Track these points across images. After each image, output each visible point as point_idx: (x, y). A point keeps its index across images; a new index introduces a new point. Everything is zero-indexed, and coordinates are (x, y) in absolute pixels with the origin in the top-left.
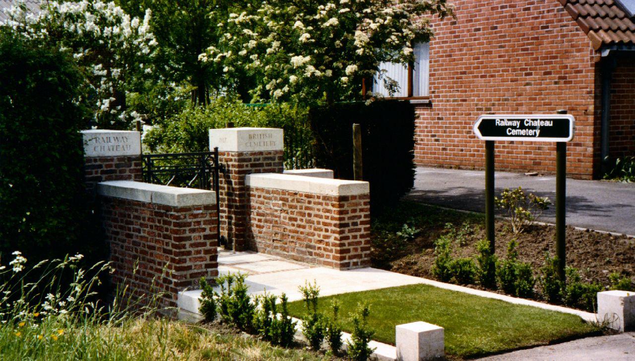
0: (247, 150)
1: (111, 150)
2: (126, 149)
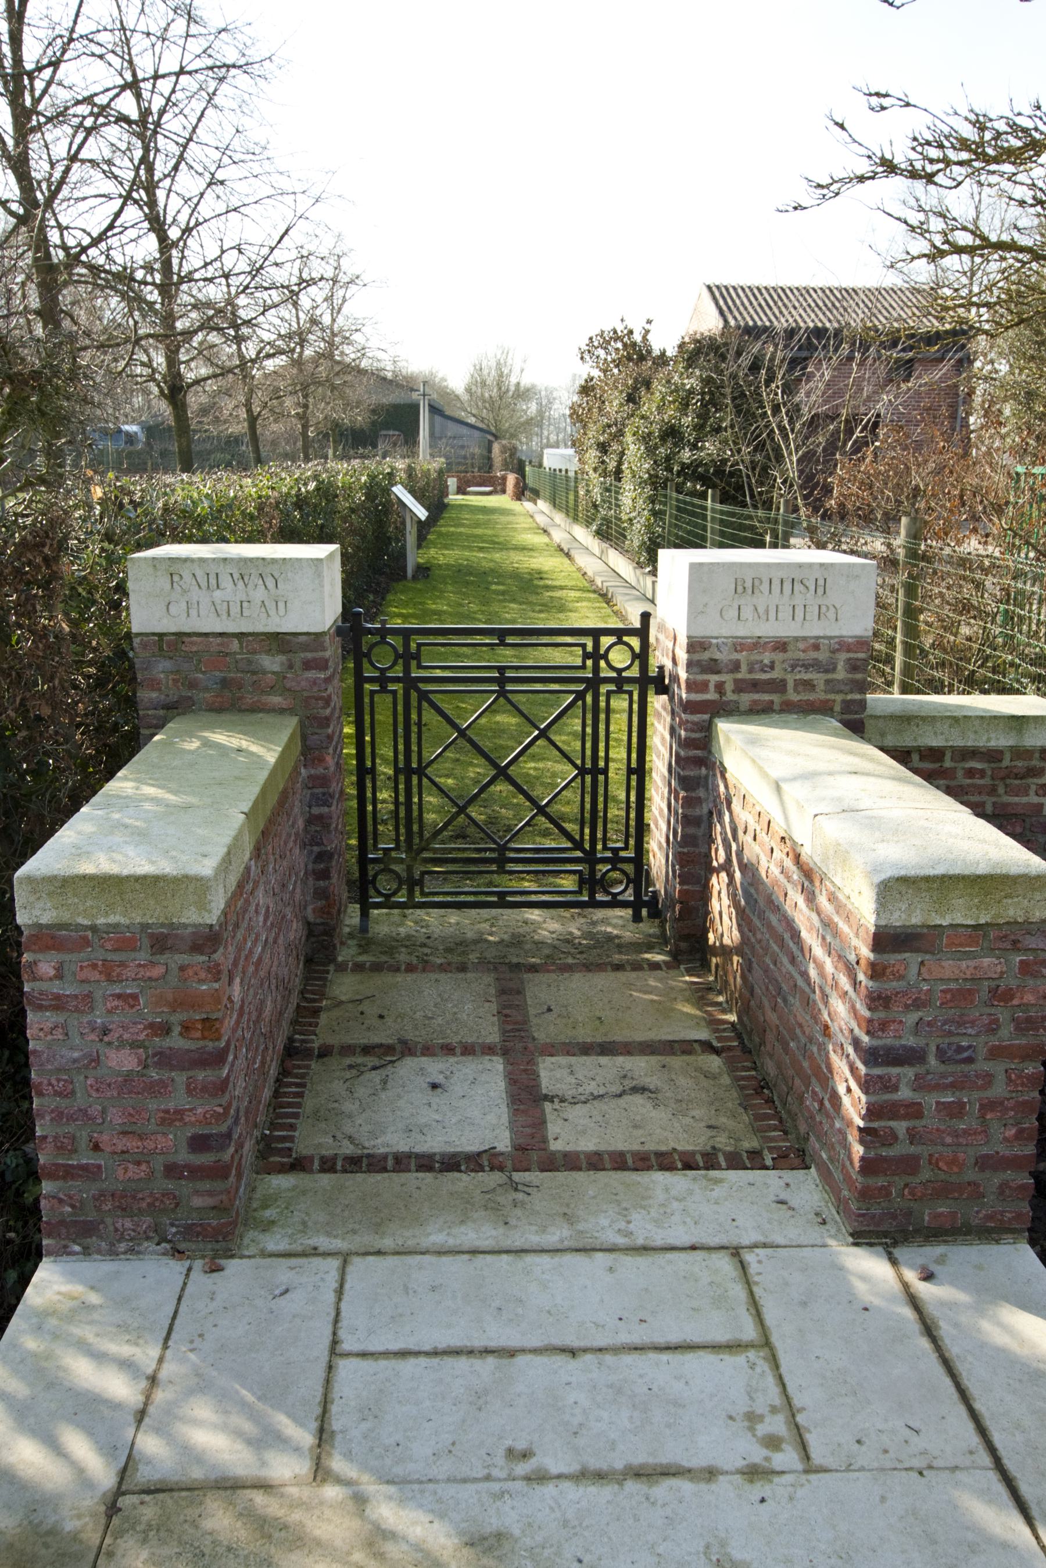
0: (725, 632)
1: (224, 616)
2: (272, 612)
